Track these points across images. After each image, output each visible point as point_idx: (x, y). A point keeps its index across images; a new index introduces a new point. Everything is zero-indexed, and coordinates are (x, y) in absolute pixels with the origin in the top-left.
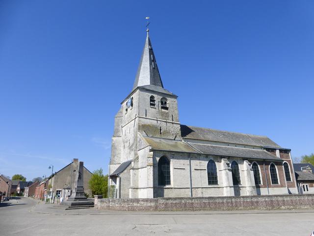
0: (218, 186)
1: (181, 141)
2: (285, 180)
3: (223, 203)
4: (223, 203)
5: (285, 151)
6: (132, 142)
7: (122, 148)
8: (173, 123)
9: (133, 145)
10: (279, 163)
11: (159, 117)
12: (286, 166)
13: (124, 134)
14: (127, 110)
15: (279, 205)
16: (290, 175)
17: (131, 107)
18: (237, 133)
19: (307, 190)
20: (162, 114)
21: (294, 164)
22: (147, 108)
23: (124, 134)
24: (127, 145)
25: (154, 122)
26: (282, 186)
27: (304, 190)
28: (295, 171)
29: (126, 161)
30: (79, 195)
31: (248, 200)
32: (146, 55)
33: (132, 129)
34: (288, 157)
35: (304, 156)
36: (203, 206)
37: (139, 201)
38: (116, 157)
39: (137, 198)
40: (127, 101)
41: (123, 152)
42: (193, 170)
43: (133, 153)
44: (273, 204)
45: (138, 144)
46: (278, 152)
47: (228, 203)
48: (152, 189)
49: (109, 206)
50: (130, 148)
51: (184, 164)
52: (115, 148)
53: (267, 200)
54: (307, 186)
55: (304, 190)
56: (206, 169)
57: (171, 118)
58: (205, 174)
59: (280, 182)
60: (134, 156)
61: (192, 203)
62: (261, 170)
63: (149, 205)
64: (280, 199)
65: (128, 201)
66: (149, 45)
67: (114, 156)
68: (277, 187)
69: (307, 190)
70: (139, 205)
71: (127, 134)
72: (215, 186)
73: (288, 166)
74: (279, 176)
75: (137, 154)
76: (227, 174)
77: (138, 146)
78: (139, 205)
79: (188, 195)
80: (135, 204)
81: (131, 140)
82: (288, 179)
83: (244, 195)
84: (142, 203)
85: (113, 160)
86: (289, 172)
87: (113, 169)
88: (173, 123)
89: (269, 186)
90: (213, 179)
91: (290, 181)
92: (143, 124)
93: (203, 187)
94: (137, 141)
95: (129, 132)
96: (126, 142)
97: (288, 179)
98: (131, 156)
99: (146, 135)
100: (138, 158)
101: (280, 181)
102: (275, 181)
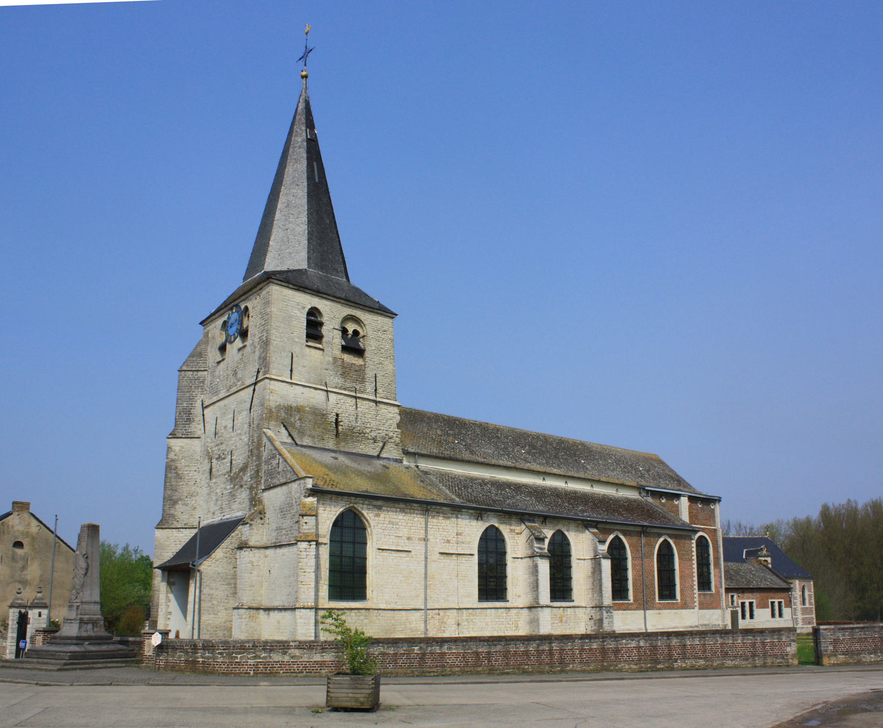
0: (508, 605)
1: (401, 461)
2: (696, 587)
3: (526, 653)
4: (526, 653)
5: (704, 502)
6: (239, 459)
7: (202, 478)
8: (376, 402)
9: (244, 469)
10: (683, 533)
11: (335, 380)
12: (702, 544)
13: (210, 428)
14: (223, 349)
15: (670, 656)
16: (709, 573)
17: (238, 343)
18: (430, 411)
19: (752, 617)
20: (346, 371)
21: (724, 539)
22: (296, 350)
23: (210, 428)
24: (220, 468)
25: (316, 398)
26: (685, 606)
27: (743, 617)
28: (725, 560)
29: (217, 519)
30: (90, 626)
31: (595, 646)
32: (296, 161)
33: (243, 418)
34: (712, 515)
35: (791, 522)
36: (471, 660)
37: (289, 647)
38: (179, 507)
39: (256, 637)
40: (225, 318)
41: (205, 491)
42: (434, 556)
43: (243, 495)
44: (660, 656)
45: (264, 467)
46: (684, 502)
47: (539, 653)
48: (647, 612)
49: (195, 662)
50: (234, 479)
51: (409, 539)
52: (179, 477)
53: (642, 644)
54: (780, 603)
55: (743, 617)
56: (328, 542)
57: (370, 387)
58: (471, 568)
59: (682, 595)
60: (247, 503)
61: (443, 654)
62: (633, 558)
63: (317, 658)
64: (675, 641)
65: (255, 646)
66: (307, 127)
67: (175, 503)
68: (627, 608)
69: (752, 617)
70: (286, 658)
71: (221, 431)
72: (571, 604)
73: (707, 546)
74: (681, 577)
75: (260, 502)
76: (535, 571)
77: (262, 474)
78: (286, 658)
79: (417, 630)
80: (276, 657)
81: (235, 453)
82: (704, 583)
83: (313, 635)
84: (297, 652)
85: (173, 516)
86: (708, 565)
87: (169, 544)
88: (376, 402)
89: (644, 604)
90: (492, 586)
91: (710, 589)
92: (281, 402)
93: (462, 607)
94: (259, 457)
95: (230, 425)
96: (219, 458)
97: (704, 583)
98: (235, 506)
99: (289, 440)
100: (262, 513)
101: (682, 591)
102: (667, 590)
